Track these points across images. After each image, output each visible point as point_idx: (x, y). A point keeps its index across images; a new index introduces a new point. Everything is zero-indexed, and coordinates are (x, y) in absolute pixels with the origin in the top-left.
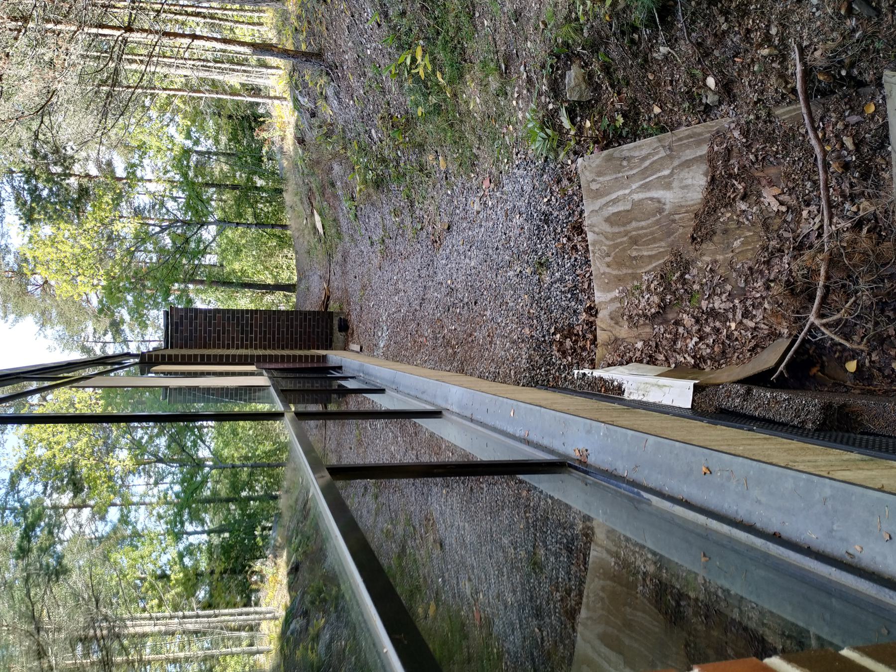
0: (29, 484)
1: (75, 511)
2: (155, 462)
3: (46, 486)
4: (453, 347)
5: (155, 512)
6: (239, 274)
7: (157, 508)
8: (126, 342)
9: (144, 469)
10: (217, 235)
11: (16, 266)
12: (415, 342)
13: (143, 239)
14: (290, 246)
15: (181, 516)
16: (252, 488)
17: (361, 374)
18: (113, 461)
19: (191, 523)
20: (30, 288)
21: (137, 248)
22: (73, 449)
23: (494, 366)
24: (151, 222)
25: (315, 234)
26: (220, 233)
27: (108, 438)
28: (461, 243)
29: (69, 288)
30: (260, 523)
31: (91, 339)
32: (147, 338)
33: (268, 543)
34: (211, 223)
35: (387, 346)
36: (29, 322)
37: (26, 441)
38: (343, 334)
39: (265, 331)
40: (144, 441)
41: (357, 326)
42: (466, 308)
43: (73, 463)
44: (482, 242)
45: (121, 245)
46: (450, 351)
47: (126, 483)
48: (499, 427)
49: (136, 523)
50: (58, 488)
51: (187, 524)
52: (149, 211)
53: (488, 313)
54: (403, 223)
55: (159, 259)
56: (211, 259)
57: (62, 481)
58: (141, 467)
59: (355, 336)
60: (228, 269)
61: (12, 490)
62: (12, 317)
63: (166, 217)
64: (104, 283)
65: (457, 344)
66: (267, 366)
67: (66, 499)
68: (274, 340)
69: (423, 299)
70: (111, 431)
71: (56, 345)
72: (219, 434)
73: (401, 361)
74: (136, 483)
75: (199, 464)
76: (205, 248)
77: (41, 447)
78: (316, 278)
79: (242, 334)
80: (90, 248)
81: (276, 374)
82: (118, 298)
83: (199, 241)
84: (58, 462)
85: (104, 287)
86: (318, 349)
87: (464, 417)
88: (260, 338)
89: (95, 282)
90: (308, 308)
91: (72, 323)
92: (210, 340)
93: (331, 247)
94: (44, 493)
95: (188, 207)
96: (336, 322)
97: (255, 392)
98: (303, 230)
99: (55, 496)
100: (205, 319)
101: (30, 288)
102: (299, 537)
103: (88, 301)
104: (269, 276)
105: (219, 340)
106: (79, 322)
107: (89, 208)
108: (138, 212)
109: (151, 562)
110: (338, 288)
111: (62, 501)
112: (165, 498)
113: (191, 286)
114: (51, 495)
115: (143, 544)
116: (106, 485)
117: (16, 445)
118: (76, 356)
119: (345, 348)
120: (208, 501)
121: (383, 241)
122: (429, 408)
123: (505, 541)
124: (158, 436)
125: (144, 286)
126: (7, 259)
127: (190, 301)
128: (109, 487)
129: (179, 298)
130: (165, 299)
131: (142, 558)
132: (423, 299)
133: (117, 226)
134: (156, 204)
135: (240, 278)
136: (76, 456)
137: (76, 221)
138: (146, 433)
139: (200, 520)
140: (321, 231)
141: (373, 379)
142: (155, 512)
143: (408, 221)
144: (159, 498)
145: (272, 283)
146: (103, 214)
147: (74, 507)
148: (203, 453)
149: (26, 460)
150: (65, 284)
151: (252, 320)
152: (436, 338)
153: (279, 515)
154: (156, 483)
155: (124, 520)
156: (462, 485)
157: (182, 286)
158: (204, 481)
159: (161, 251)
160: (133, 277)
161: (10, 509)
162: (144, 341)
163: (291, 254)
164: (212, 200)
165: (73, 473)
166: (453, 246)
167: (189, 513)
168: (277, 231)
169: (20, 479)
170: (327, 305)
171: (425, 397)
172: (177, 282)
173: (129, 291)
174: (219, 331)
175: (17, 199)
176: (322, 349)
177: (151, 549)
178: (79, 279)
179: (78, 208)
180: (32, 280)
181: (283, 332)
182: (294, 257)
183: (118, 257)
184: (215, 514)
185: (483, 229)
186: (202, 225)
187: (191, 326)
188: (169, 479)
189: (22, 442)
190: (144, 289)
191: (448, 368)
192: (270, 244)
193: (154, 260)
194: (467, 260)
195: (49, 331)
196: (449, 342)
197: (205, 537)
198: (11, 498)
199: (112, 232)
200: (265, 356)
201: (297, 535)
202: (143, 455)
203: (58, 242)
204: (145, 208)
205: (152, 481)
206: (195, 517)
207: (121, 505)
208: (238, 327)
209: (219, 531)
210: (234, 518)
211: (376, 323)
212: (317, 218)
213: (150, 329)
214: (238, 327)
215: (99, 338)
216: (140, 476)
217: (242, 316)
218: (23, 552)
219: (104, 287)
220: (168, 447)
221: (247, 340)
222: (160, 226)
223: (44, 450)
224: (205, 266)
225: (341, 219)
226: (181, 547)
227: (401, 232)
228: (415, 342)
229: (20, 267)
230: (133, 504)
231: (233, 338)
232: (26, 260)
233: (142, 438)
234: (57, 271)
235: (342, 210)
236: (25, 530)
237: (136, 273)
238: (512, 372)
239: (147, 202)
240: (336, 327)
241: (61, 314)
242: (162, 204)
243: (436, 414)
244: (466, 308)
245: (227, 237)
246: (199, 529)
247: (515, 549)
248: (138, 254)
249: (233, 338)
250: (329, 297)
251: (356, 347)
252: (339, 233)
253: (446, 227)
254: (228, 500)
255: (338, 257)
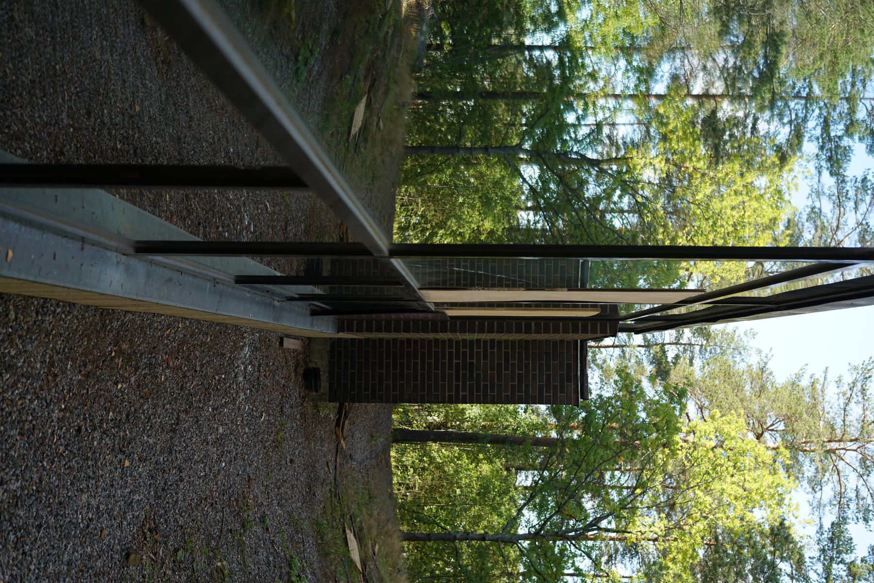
0: (776, 134)
1: (713, 91)
2: (602, 161)
3: (754, 128)
4: (120, 352)
5: (601, 83)
6: (481, 456)
7: (597, 89)
8: (648, 346)
9: (618, 149)
10: (515, 519)
11: (801, 459)
12: (188, 359)
13: (624, 508)
14: (402, 506)
15: (563, 76)
16: (459, 114)
17: (276, 303)
18: (661, 165)
19: (549, 63)
20: (781, 427)
21: (633, 493)
22: (718, 184)
23: (46, 325)
24: (613, 535)
25: (361, 529)
26: (513, 522)
27: (669, 198)
28: (106, 532)
29: (726, 428)
30: (445, 58)
31: (697, 348)
32: (618, 351)
33: (431, 26)
34: (525, 537)
35: (237, 348)
36: (781, 375)
37: (781, 198)
38: (311, 365)
39: (436, 368)
40: (618, 192)
41: (288, 379)
42: (96, 421)
43: (717, 163)
44: (67, 537)
45: (656, 496)
46: (125, 346)
47: (643, 128)
48: (34, 231)
49: (627, 71)
50: (736, 125)
51: (555, 62)
52: (617, 550)
53: (56, 415)
54: (209, 558)
55: (602, 476)
56: (525, 479)
57: (731, 136)
58: (622, 152)
59: (291, 363)
60: (498, 463)
61: (798, 124)
62: (805, 382)
63: (590, 543)
64: (677, 438)
65: (113, 358)
66: (430, 316)
67: (726, 109)
68: (423, 354)
69: (174, 431)
70: (664, 208)
71: (745, 339)
72: (508, 200)
73: (212, 324)
74: (629, 129)
75: (537, 156)
76: (532, 497)
77: (759, 189)
78: (358, 456)
79: (471, 364)
80: (698, 492)
81: (415, 305)
82: (656, 415)
83: (541, 509)
84: (737, 167)
85: (678, 430)
86: (353, 340)
87: (93, 244)
88: (444, 357)
89: (691, 438)
90: (372, 407)
91: (721, 375)
92: (520, 353)
93: (334, 509)
94: (756, 120)
95: (559, 561)
96: (324, 385)
97: (444, 282)
98: (379, 534)
99: (740, 114)
100: (527, 386)
101: (781, 427)
102: (381, 35)
103: (701, 408)
104: (435, 454)
105: (506, 354)
106: (712, 376)
107: (701, 552)
108: (632, 549)
109: (605, 9)
110: (322, 439)
111: (729, 108)
112: (586, 104)
113: (554, 434)
114: (746, 116)
115: (616, 37)
116: (670, 127)
117: (793, 192)
118: (716, 328)
119: (309, 342)
120: (524, 96)
121: (243, 526)
122: (160, 258)
123: (29, 31)
124: (598, 199)
125: (622, 434)
126: (813, 469)
127: (555, 412)
128: (666, 125)
129: (572, 417)
130: (590, 413)
131: (617, 16)
132: (174, 431)
133: (660, 525)
134: (607, 563)
135: (480, 452)
136: (712, 174)
137: (719, 531)
138: (615, 203)
139: (535, 66)
140: (350, 536)
141: (258, 298)
142: (601, 83)
143: (200, 563)
144: (594, 104)
145: (430, 443)
146: (681, 545)
147: (714, 96)
148: (531, 172)
149: (781, 169)
150: (733, 434)
151: (457, 386)
152: (150, 366)
153: (415, 68)
154: (599, 126)
155: (647, 73)
156: (106, 120)
157: (566, 435)
158: (531, 125)
159: (598, 489)
160: (636, 448)
161: (801, 98)
162: (622, 346)
163: (399, 492)
164: (523, 574)
165: (716, 148)
166: (120, 525)
167: (552, 78)
168: (423, 529)
169: (788, 140)
170: (340, 412)
171: (167, 273)
172: (574, 441)
173: (644, 426)
174: (507, 369)
175: (800, 562)
176: (346, 340)
177: (605, 29)
178: (713, 443)
179: (717, 552)
180: (779, 439)
181: (409, 368)
182: (396, 487)
183: (660, 478)
184: (513, 75)
185: (66, 558)
186: (537, 533)
187: (548, 376)
188: (583, 131)
189: (786, 197)
190: (621, 428)
191: (129, 316)
192: (433, 507)
193: (607, 476)
194: (93, 502)
195: (754, 360)
196: (128, 360)
197: (528, 41)
198: (801, 115)
199: (668, 516)
200: (435, 330)
201: (385, 37)
202: (619, 172)
203: (743, 498)
204: (623, 555)
205: (606, 130)
206: (544, 70)
207: (649, 96)
208: (478, 375)
209: (507, 48)
210: (484, 66)
211: (256, 385)
212: (356, 555)
213: (612, 364)
214: (478, 375)
215: (685, 350)
216: (623, 138)
217: (471, 393)
218: (774, 42)
219: (678, 430)
220: (583, 183)
221: (465, 353)
222: (599, 529)
223: (757, 183)
224: (534, 468)
225: (314, 557)
226: (561, 30)
227: (213, 543)
228: (188, 359)
229: (794, 458)
230: (631, 97)
231: (485, 358)
232: (787, 468)
233: (620, 197)
234: (743, 453)
235: (313, 573)
236: (772, 76)
237: (634, 455)
238: (12, 315)
239: (619, 565)
240: (324, 377)
241: (738, 388)
242: (596, 563)
243: (145, 248)
244: (96, 421)
245: (500, 515)
246: (537, 53)
247: (12, 18)
248: (632, 482)
249: (485, 358)
250: (337, 425)
251: (289, 344)
252: (320, 534)
253: (132, 557)
254: (493, 95)
255: (321, 493)
